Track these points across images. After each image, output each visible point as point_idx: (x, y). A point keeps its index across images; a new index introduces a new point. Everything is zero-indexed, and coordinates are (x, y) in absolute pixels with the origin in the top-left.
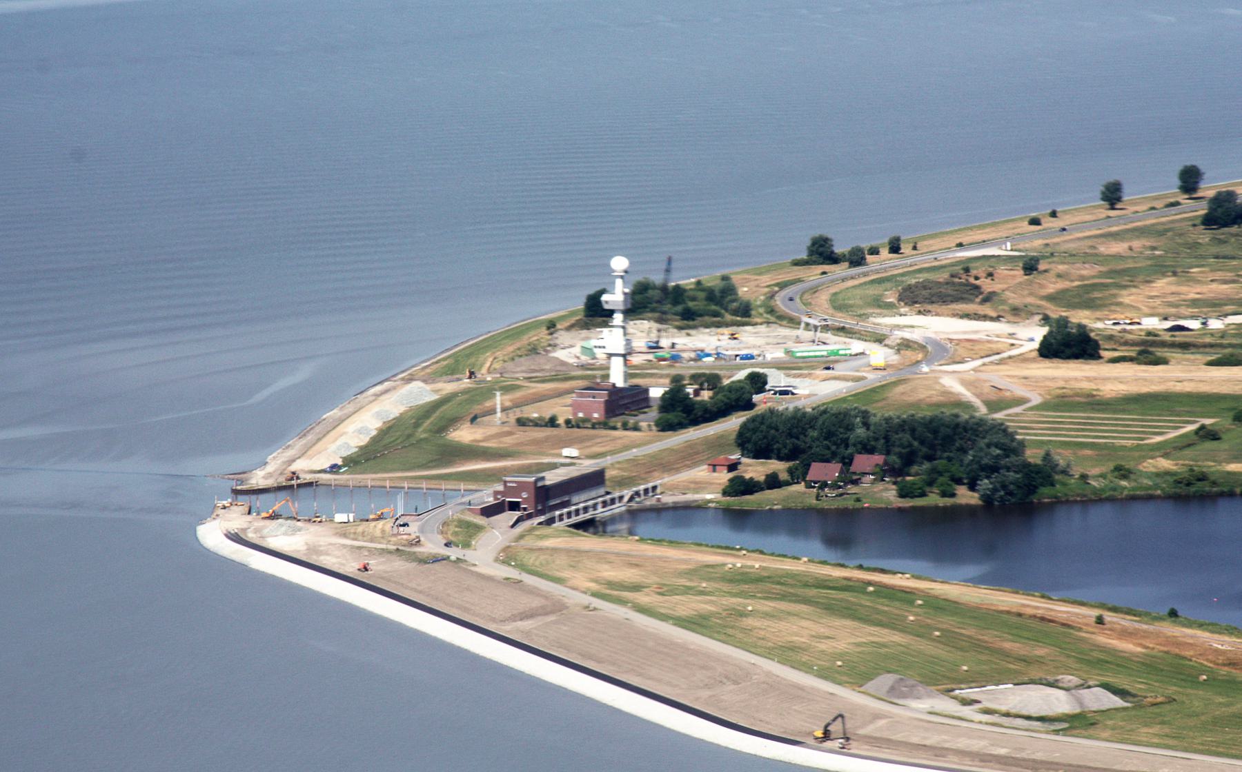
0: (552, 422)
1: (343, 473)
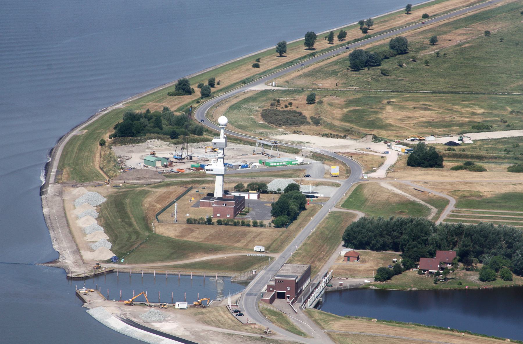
0: (209, 222)
1: (124, 263)
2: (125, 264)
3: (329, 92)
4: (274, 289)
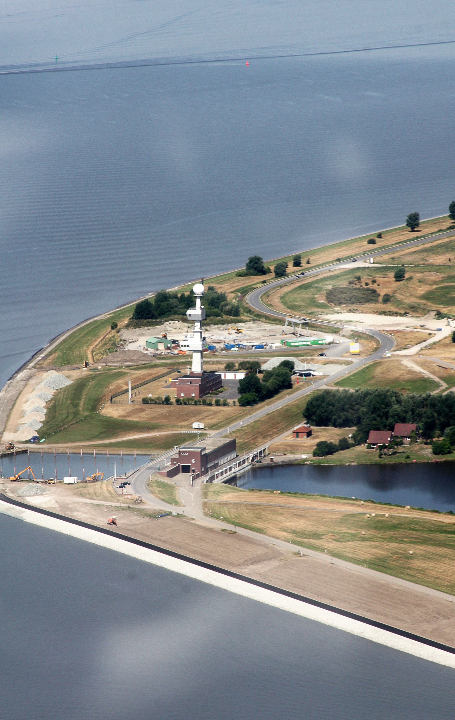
0: (167, 401)
1: (43, 443)
2: (43, 444)
3: (434, 268)
4: (178, 462)
